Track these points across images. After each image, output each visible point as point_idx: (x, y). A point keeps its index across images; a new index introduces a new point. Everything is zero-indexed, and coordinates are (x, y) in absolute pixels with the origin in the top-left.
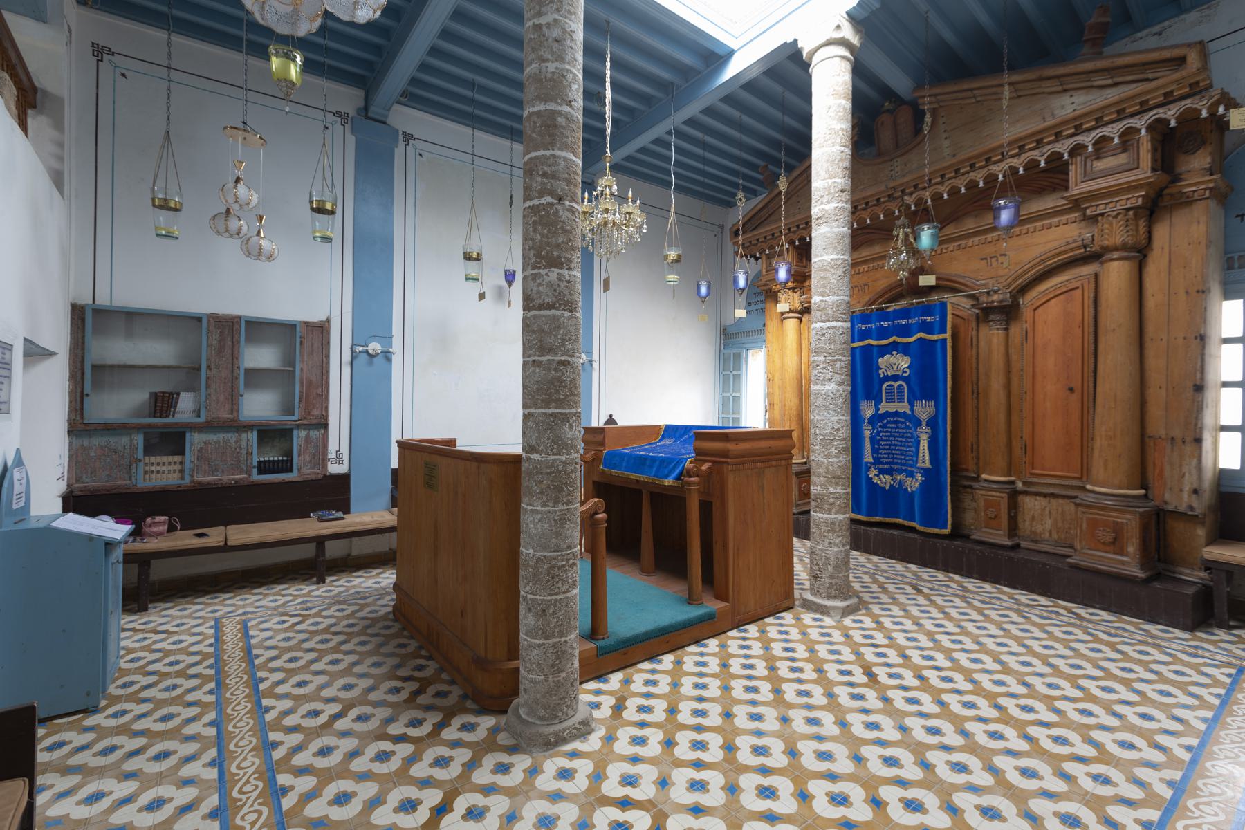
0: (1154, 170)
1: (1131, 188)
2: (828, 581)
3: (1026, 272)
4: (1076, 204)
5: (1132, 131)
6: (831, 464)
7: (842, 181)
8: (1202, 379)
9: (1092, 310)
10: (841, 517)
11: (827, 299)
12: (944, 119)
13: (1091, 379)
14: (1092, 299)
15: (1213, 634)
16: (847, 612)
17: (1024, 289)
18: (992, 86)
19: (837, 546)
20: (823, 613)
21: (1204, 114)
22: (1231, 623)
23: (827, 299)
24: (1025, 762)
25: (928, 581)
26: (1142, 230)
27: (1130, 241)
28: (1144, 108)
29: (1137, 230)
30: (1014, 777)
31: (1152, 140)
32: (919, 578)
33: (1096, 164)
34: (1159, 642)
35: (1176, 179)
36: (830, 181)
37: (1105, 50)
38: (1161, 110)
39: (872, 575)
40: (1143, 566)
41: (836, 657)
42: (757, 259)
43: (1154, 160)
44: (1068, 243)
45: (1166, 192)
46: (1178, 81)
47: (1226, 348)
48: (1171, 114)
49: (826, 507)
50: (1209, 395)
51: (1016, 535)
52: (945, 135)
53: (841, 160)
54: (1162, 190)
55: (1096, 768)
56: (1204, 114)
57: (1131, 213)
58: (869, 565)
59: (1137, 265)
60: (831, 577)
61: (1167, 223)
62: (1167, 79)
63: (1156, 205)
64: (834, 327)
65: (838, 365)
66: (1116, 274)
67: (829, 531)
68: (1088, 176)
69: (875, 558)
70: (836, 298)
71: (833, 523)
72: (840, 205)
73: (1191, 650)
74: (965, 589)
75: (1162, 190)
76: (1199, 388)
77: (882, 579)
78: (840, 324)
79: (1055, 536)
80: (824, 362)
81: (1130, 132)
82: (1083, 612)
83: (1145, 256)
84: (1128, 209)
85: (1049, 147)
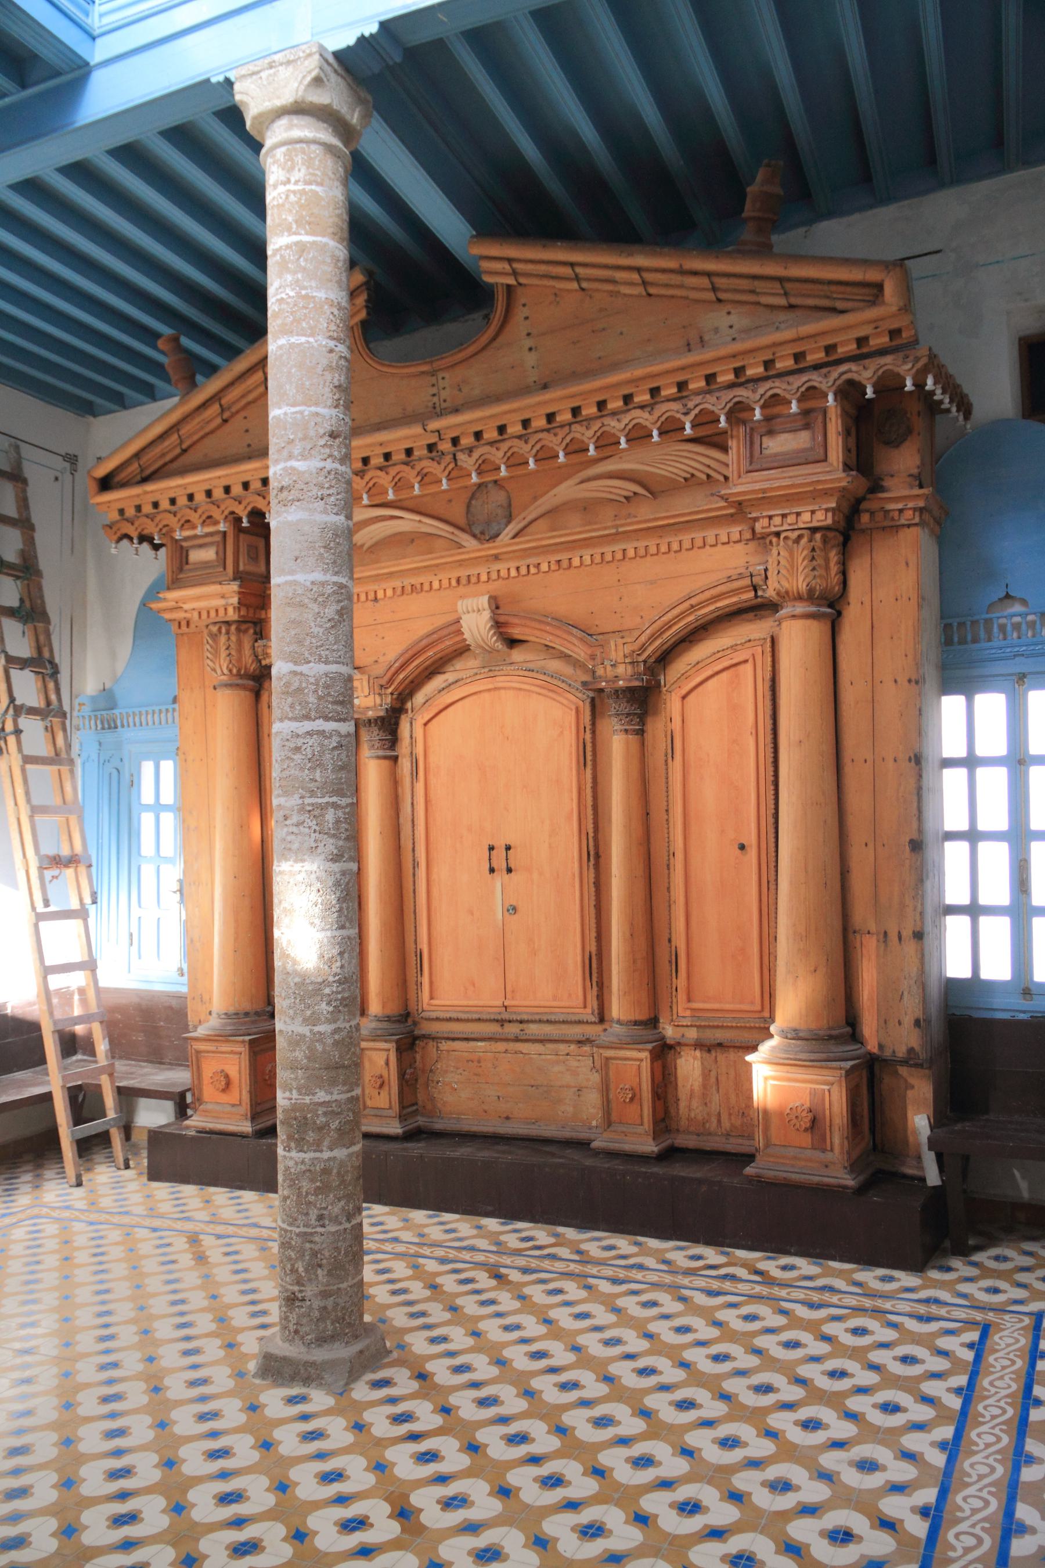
0: (847, 467)
1: (817, 494)
2: (317, 1303)
3: (668, 626)
4: (740, 510)
5: (811, 393)
6: (320, 1037)
7: (327, 413)
8: (920, 831)
9: (768, 703)
10: (341, 1153)
11: (304, 668)
12: (525, 312)
13: (771, 830)
14: (768, 684)
15: (949, 1269)
16: (355, 1370)
17: (665, 658)
18: (606, 267)
19: (336, 1220)
20: (307, 1381)
21: (909, 386)
22: (971, 1242)
23: (304, 668)
24: (805, 1413)
25: (518, 1252)
26: (834, 569)
27: (819, 585)
28: (832, 360)
29: (827, 568)
30: (824, 1383)
31: (845, 414)
32: (502, 1249)
33: (767, 442)
34: (879, 1303)
35: (876, 487)
36: (308, 410)
37: (774, 238)
38: (853, 366)
39: (413, 1260)
40: (853, 1167)
41: (421, 1321)
42: (156, 547)
43: (847, 450)
44: (730, 579)
45: (864, 505)
46: (875, 322)
47: (947, 773)
48: (866, 376)
49: (311, 1136)
50: (930, 853)
51: (668, 1130)
52: (528, 343)
53: (329, 368)
54: (859, 501)
55: (916, 1370)
56: (909, 386)
57: (818, 536)
58: (406, 1236)
59: (826, 627)
60: (325, 1295)
61: (866, 560)
62: (860, 321)
63: (849, 530)
64: (321, 733)
65: (330, 816)
66: (798, 639)
67: (318, 1191)
68: (756, 463)
69: (419, 1216)
70: (322, 668)
71: (326, 1171)
72: (329, 465)
73: (922, 1309)
74: (584, 1258)
75: (859, 501)
76: (917, 846)
77: (431, 1266)
78: (330, 726)
79: (726, 1124)
80: (302, 809)
81: (811, 393)
82: (772, 1266)
83: (839, 614)
84: (814, 530)
85: (697, 399)
